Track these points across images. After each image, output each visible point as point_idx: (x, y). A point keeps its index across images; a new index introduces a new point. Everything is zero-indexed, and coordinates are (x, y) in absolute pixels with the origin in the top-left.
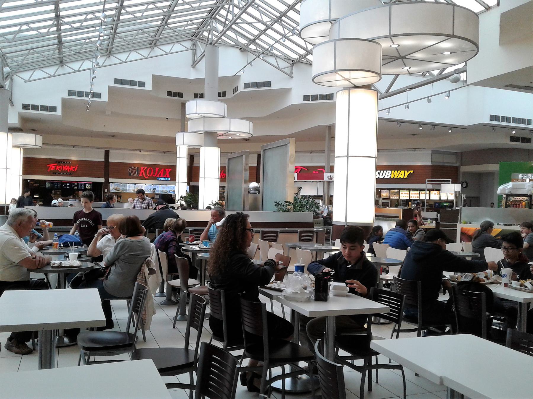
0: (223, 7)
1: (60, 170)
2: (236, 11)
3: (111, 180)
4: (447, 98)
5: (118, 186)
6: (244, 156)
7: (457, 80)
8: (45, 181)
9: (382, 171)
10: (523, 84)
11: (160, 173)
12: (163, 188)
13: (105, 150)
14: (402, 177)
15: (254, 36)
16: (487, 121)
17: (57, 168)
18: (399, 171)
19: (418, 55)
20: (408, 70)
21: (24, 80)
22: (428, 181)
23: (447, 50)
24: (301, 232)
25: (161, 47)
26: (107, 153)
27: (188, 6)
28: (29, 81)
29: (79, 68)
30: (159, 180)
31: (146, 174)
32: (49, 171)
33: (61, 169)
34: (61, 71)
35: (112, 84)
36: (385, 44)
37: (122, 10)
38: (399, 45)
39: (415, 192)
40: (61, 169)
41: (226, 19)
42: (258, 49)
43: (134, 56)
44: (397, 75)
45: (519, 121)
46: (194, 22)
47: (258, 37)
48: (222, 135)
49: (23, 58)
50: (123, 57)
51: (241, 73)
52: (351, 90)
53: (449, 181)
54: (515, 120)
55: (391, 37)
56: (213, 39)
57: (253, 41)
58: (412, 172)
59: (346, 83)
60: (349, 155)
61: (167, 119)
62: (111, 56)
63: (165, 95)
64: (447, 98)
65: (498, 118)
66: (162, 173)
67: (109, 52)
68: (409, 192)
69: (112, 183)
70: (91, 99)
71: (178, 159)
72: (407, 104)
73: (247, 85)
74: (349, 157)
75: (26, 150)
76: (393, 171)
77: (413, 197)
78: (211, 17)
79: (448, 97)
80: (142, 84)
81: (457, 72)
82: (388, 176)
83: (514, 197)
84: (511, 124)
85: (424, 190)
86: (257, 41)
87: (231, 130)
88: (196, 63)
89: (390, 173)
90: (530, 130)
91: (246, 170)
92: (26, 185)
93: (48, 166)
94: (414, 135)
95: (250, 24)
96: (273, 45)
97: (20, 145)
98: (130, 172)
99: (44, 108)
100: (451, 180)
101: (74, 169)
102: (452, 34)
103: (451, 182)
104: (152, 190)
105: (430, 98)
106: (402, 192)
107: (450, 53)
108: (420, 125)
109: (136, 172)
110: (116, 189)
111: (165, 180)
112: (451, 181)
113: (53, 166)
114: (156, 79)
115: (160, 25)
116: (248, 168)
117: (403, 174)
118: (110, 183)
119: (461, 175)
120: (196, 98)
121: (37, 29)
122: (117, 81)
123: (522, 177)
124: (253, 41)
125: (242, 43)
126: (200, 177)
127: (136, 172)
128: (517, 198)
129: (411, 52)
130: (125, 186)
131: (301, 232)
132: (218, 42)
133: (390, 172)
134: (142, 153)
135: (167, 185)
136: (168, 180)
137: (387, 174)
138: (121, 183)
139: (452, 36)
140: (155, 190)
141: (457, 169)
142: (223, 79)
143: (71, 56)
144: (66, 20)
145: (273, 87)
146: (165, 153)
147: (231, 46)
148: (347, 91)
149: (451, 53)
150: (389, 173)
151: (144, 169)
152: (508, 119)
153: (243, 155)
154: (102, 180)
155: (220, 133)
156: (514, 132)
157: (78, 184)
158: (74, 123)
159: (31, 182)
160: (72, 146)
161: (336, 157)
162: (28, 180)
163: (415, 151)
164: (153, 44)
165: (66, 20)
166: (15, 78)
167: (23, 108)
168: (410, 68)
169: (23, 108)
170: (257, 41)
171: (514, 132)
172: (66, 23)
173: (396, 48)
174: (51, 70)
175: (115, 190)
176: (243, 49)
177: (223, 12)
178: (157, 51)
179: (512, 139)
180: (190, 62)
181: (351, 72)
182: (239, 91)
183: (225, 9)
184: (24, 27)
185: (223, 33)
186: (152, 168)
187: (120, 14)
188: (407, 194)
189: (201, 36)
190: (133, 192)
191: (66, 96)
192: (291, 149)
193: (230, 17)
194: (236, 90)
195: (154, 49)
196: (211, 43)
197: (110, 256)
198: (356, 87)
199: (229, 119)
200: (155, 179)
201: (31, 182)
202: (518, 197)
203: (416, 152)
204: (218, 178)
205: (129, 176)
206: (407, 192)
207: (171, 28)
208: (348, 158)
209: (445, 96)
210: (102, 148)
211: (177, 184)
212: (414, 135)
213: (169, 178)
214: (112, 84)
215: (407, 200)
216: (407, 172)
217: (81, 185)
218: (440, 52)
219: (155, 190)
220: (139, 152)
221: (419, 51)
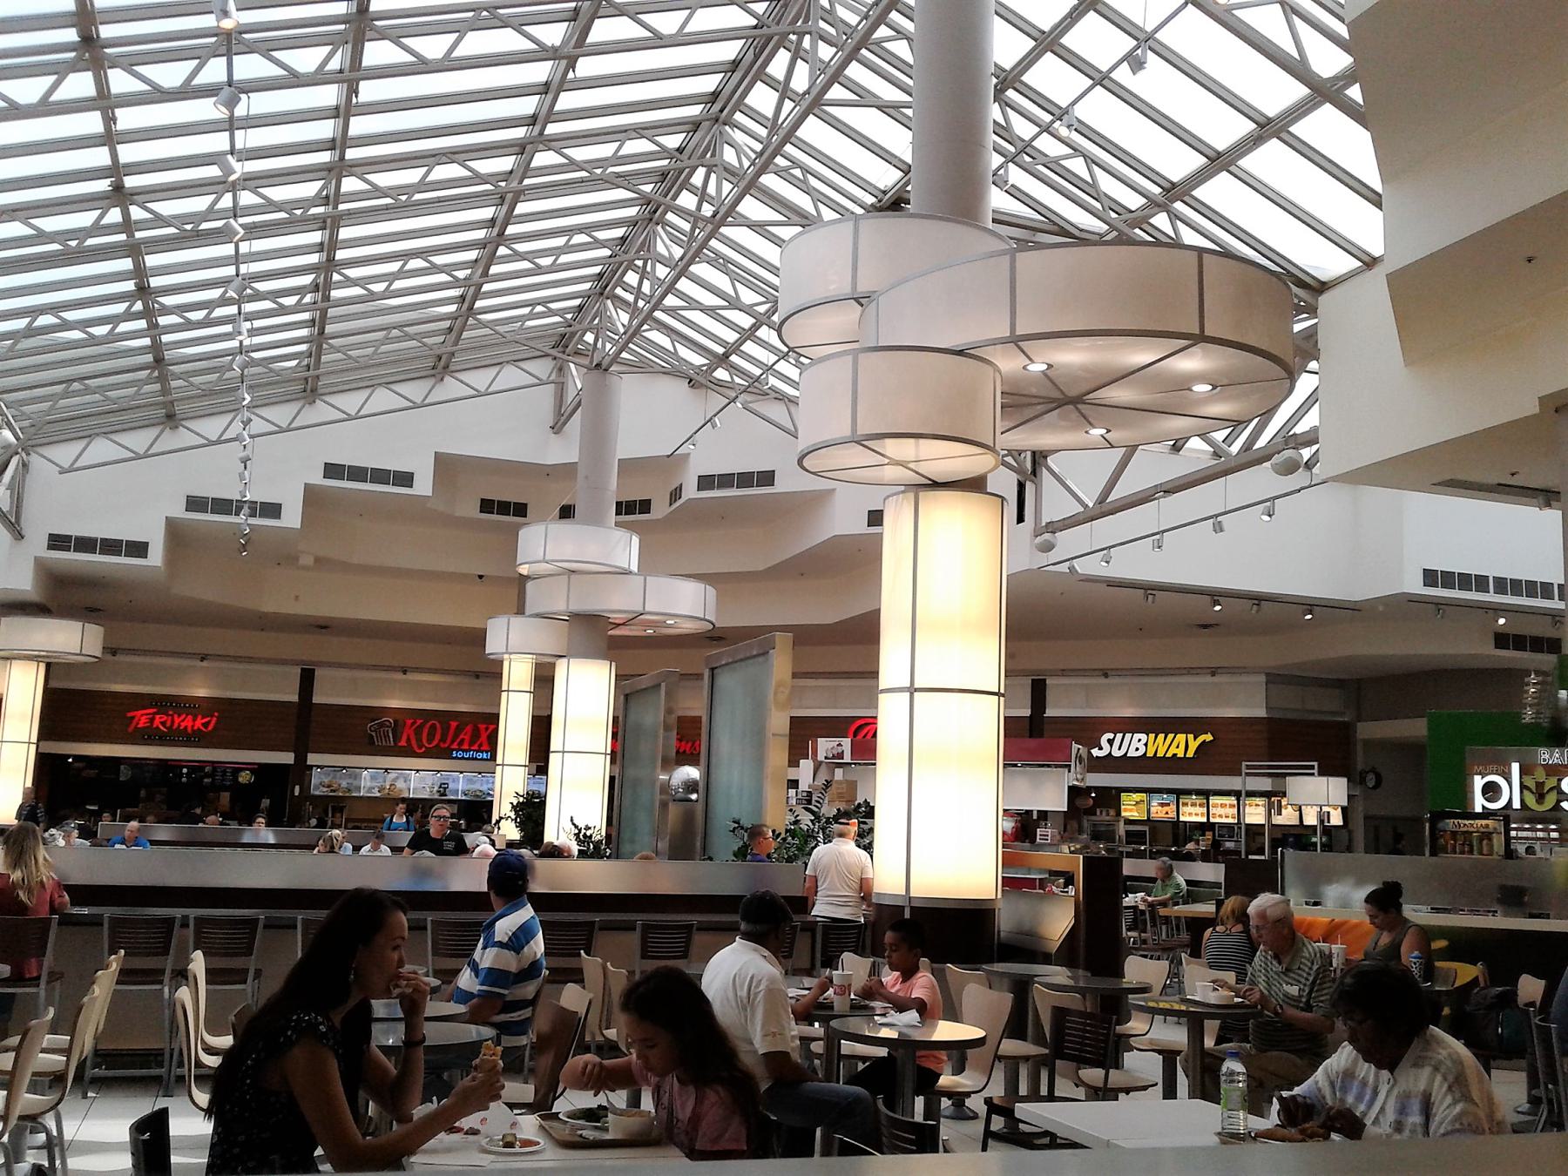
0: (631, 266)
1: (165, 727)
2: (662, 271)
3: (312, 759)
4: (1267, 518)
5: (334, 777)
6: (663, 684)
7: (1290, 468)
8: (117, 761)
9: (1119, 736)
10: (1494, 479)
11: (462, 736)
12: (470, 781)
13: (302, 669)
14: (1181, 755)
15: (725, 344)
16: (1415, 586)
17: (157, 722)
18: (1171, 736)
19: (1119, 394)
20: (1105, 436)
21: (57, 465)
22: (1248, 767)
23: (1200, 378)
24: (647, 928)
25: (462, 376)
26: (307, 679)
27: (526, 265)
28: (71, 469)
29: (221, 435)
30: (456, 758)
31: (419, 740)
32: (130, 730)
33: (168, 724)
34: (171, 440)
35: (318, 479)
36: (1009, 363)
37: (334, 274)
38: (1050, 366)
39: (1224, 802)
40: (168, 724)
41: (638, 292)
42: (737, 380)
43: (383, 398)
44: (1132, 449)
45: (1516, 586)
46: (553, 306)
47: (735, 348)
48: (623, 624)
49: (45, 406)
50: (350, 402)
51: (689, 447)
52: (921, 494)
53: (1312, 767)
54: (1501, 585)
55: (1016, 341)
56: (607, 350)
57: (723, 360)
58: (1209, 737)
59: (908, 476)
60: (916, 686)
61: (481, 577)
62: (317, 401)
63: (474, 511)
64: (1266, 518)
65: (1448, 579)
66: (467, 738)
67: (309, 388)
68: (1235, 802)
69: (318, 767)
70: (249, 522)
71: (504, 695)
72: (1158, 537)
73: (705, 482)
74: (916, 690)
75: (53, 668)
76: (1152, 736)
77: (1220, 816)
78: (602, 294)
79: (1270, 516)
80: (406, 479)
81: (1293, 445)
82: (1137, 749)
83: (1456, 821)
84: (1491, 597)
85: (1188, 792)
86: (734, 358)
87: (647, 609)
88: (563, 418)
89: (1144, 741)
90: (1555, 617)
91: (667, 728)
92: (47, 767)
93: (129, 715)
94: (1205, 626)
95: (670, 313)
96: (774, 364)
97: (36, 653)
98: (374, 734)
99: (111, 547)
100: (1315, 764)
101: (206, 725)
102: (1197, 331)
103: (1315, 771)
104: (436, 789)
105: (1219, 519)
106: (1186, 801)
107: (1210, 387)
108: (1216, 598)
109: (391, 735)
110: (329, 787)
111: (476, 759)
112: (1316, 767)
113: (145, 717)
114: (446, 466)
115: (456, 315)
116: (673, 719)
117: (1181, 745)
118: (312, 766)
119: (1359, 748)
120: (564, 518)
121: (84, 324)
122: (332, 470)
123: (1547, 756)
124: (723, 360)
125: (692, 364)
126: (551, 750)
127: (391, 735)
128: (1465, 825)
129: (1093, 386)
130: (357, 777)
131: (647, 928)
132: (619, 360)
133: (1143, 737)
134: (411, 676)
135: (480, 773)
136: (485, 757)
137: (1135, 744)
138: (344, 768)
139: (1200, 338)
140: (445, 788)
141: (1346, 730)
142: (629, 467)
143: (191, 401)
144: (169, 301)
145: (781, 486)
146: (477, 677)
147: (664, 373)
148: (911, 496)
149: (1214, 387)
150: (1140, 740)
151: (412, 724)
152: (1481, 583)
153: (660, 685)
154: (287, 758)
155: (615, 618)
156: (1502, 621)
157: (214, 769)
158: (203, 588)
159: (76, 765)
160: (1101, 673)
161: (883, 691)
162: (69, 756)
163: (1213, 674)
164: (441, 367)
165: (169, 301)
166: (35, 460)
167: (50, 547)
168: (1108, 431)
169: (50, 547)
170: (734, 358)
171: (1502, 621)
172: (166, 311)
173: (1043, 372)
174: (139, 440)
175: (325, 789)
176: (697, 381)
177: (632, 278)
178: (451, 387)
179: (1501, 640)
180: (549, 420)
181: (922, 441)
182: (685, 497)
183: (635, 269)
184: (46, 320)
185: (633, 334)
186: (438, 725)
187: (329, 285)
188: (1232, 806)
189: (579, 346)
190: (378, 795)
191: (179, 511)
192: (780, 664)
193: (646, 288)
194: (676, 494)
195: (445, 379)
196: (598, 365)
197: (731, 995)
198: (935, 485)
199: (642, 578)
200: (445, 754)
201: (76, 765)
202: (1467, 822)
203: (1216, 679)
204: (606, 754)
205: (372, 748)
206: (1232, 800)
207: (484, 325)
208: (916, 690)
209: (1263, 514)
210: (295, 663)
211: (499, 769)
212: (1205, 626)
213: (487, 752)
214: (318, 479)
215: (1202, 824)
216: (1195, 738)
217: (224, 772)
218: (1183, 384)
219: (445, 788)
220: (400, 676)
221: (1123, 377)
